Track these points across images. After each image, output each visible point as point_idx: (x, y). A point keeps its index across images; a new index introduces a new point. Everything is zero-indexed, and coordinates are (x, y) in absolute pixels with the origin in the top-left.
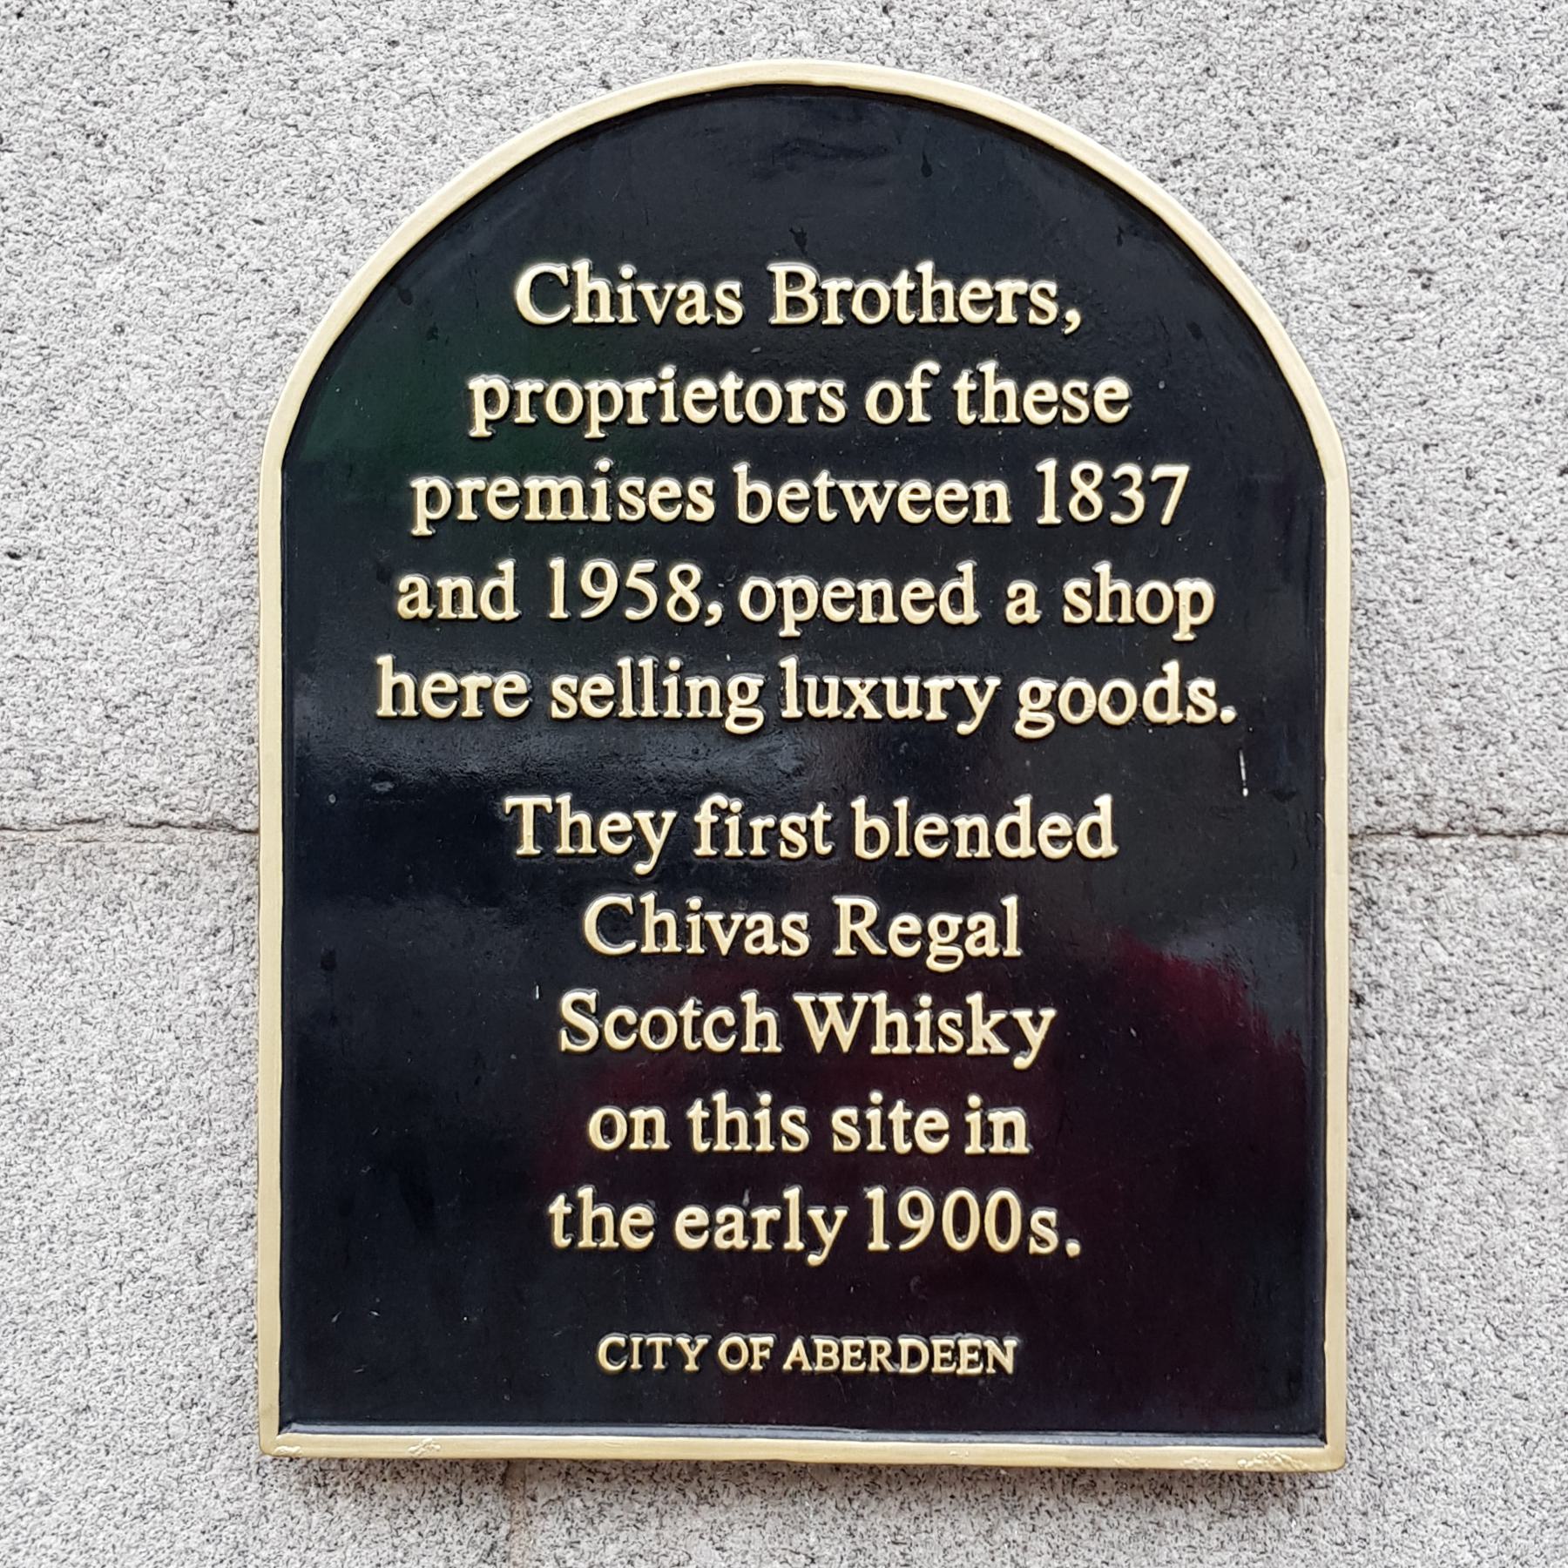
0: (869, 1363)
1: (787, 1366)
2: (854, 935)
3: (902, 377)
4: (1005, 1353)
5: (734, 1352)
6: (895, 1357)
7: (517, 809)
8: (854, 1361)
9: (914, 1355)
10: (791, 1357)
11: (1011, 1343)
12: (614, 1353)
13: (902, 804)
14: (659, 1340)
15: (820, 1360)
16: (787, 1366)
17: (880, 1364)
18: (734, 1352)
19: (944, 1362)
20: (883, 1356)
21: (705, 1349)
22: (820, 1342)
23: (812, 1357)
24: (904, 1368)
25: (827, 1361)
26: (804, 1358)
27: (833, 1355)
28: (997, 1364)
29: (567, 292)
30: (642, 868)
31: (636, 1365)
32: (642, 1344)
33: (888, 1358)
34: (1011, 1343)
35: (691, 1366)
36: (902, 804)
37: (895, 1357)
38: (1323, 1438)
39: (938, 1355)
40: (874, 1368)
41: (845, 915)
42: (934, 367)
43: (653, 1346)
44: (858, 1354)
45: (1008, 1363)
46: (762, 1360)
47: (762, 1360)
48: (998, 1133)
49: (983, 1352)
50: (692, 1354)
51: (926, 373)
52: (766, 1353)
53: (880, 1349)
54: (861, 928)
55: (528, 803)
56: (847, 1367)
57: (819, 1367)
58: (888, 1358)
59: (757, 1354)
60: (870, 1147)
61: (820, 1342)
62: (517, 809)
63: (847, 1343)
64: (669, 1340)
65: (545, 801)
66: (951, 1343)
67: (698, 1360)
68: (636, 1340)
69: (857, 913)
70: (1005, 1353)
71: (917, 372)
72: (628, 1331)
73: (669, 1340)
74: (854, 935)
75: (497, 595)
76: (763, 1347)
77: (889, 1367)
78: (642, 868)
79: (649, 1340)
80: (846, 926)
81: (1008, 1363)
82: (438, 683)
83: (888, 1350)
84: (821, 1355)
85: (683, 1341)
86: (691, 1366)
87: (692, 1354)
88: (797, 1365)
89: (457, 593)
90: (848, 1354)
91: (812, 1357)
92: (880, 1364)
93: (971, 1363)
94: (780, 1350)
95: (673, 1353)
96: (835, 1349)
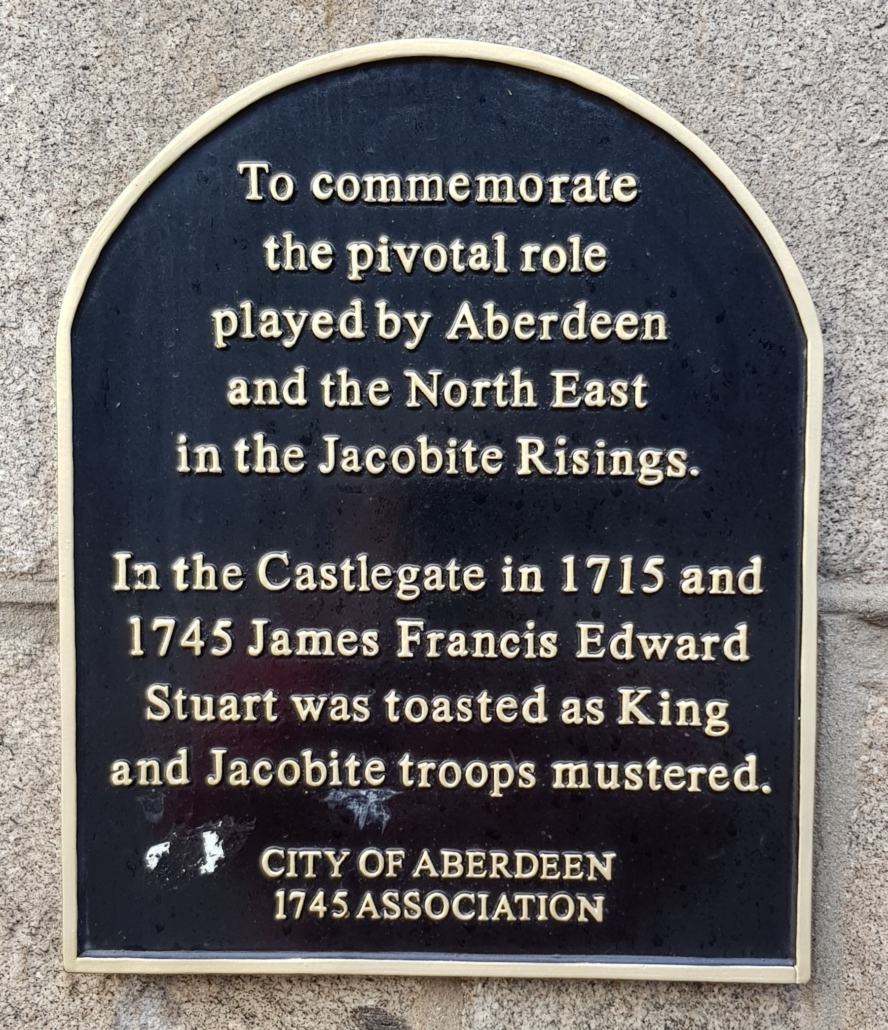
0: (563, 872)
2: (530, 461)
6: (511, 866)
8: (550, 871)
11: (609, 856)
14: (311, 854)
17: (499, 871)
18: (371, 863)
20: (501, 866)
22: (446, 854)
23: (439, 866)
25: (452, 869)
27: (458, 864)
29: (475, 906)
33: (506, 867)
34: (609, 856)
37: (511, 866)
39: (546, 866)
40: (494, 875)
41: (525, 449)
43: (305, 857)
44: (480, 864)
47: (396, 868)
48: (716, 581)
49: (586, 862)
52: (399, 863)
53: (500, 860)
54: (535, 457)
56: (470, 874)
57: (446, 874)
58: (506, 867)
59: (391, 864)
60: (468, 875)
61: (446, 854)
63: (471, 855)
64: (318, 853)
67: (340, 867)
69: (533, 447)
73: (318, 853)
74: (530, 461)
75: (293, 389)
76: (550, 861)
77: (507, 875)
80: (525, 456)
82: (346, 637)
83: (506, 861)
84: (447, 864)
85: (330, 854)
87: (337, 864)
89: (266, 388)
90: (472, 865)
91: (439, 866)
92: (499, 871)
96: (459, 858)
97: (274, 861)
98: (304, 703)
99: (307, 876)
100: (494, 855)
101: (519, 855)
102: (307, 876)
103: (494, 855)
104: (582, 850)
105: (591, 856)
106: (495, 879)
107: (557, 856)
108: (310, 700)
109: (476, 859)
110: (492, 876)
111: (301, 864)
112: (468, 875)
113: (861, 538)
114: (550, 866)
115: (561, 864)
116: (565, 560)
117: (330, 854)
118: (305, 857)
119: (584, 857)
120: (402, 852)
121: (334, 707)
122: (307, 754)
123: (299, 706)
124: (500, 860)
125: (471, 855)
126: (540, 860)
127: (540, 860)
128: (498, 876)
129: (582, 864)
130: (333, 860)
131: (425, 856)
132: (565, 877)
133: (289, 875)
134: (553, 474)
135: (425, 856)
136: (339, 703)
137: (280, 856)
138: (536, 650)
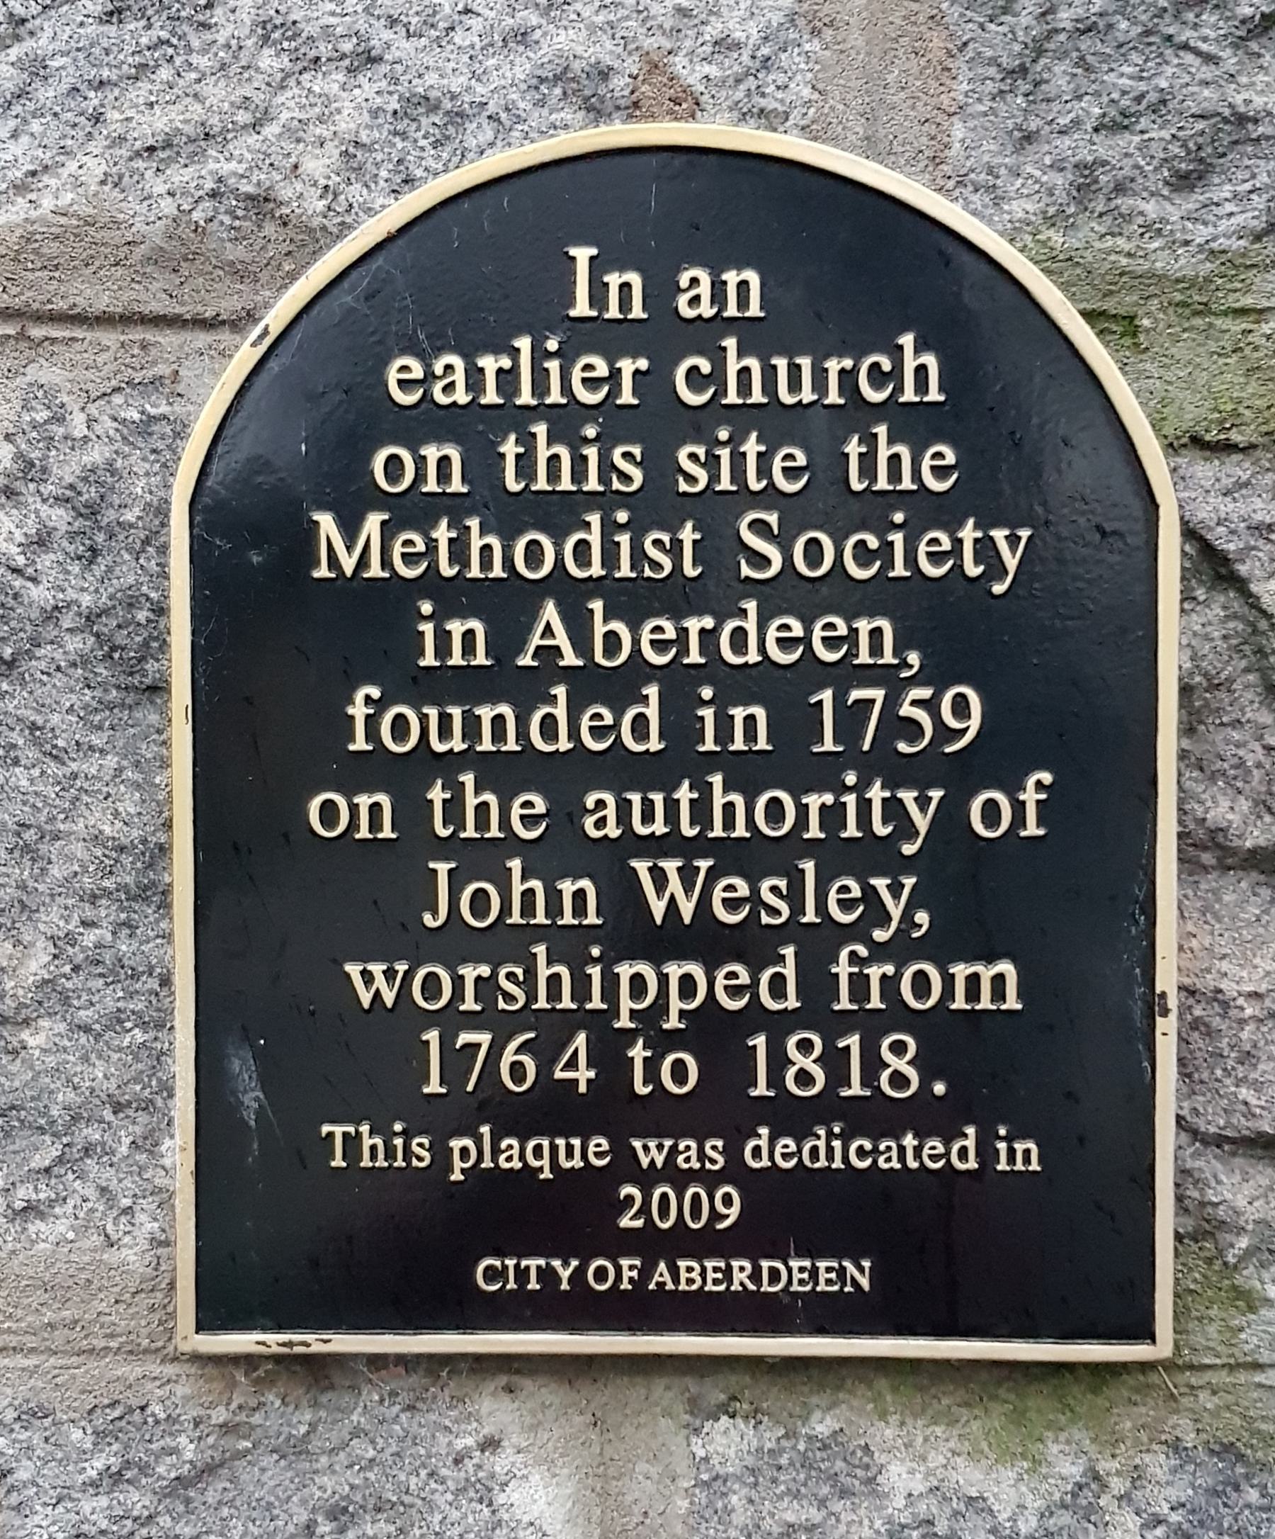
0: (817, 1284)
1: (652, 1286)
3: (1013, 788)
4: (861, 1275)
5: (601, 1274)
7: (331, 1135)
8: (716, 1282)
9: (774, 1275)
10: (656, 1278)
12: (491, 1274)
13: (485, 1130)
15: (683, 1281)
16: (652, 1286)
17: (742, 1284)
18: (601, 1274)
19: (716, 1282)
20: (743, 1276)
21: (576, 1269)
22: (682, 1264)
23: (676, 1281)
24: (766, 1288)
25: (690, 1281)
26: (667, 1278)
28: (854, 1282)
30: (909, 849)
31: (511, 1285)
32: (517, 1266)
35: (565, 1286)
36: (485, 1130)
38: (1154, 1341)
39: (797, 1276)
40: (736, 1287)
42: (1047, 778)
45: (865, 1282)
46: (631, 1280)
47: (631, 1280)
49: (842, 1272)
50: (565, 1274)
51: (1039, 784)
52: (635, 1274)
53: (742, 1269)
55: (338, 1130)
56: (709, 1287)
59: (627, 1274)
60: (706, 1289)
61: (682, 1264)
62: (331, 1135)
63: (709, 1265)
65: (351, 1129)
66: (722, 1265)
67: (570, 1280)
68: (510, 1263)
70: (861, 1275)
71: (1031, 783)
72: (500, 1253)
73: (542, 1262)
76: (631, 1268)
77: (752, 1287)
78: (909, 849)
79: (524, 1263)
81: (865, 1282)
84: (684, 1275)
85: (556, 1263)
86: (565, 1286)
87: (565, 1274)
88: (661, 1285)
90: (711, 1275)
91: (676, 1281)
92: (742, 1284)
93: (716, 1282)
94: (646, 1272)
95: (547, 1275)
97: (491, 1274)
98: (646, 1148)
99: (530, 1287)
100: (736, 1264)
101: (765, 1264)
102: (530, 1287)
103: (736, 1264)
104: (839, 1256)
105: (847, 1264)
106: (736, 1292)
107: (835, 1265)
108: (652, 1144)
109: (829, 1270)
110: (733, 1288)
111: (522, 1274)
112: (706, 1289)
113: (459, 120)
114: (688, 1275)
115: (814, 1272)
116: (510, 864)
117: (556, 1263)
118: (527, 1268)
119: (840, 1265)
120: (638, 1263)
121: (682, 1153)
122: (546, 1174)
123: (640, 1153)
124: (690, 1270)
125: (625, 1263)
126: (790, 1270)
127: (790, 1270)
128: (740, 1288)
129: (810, 1272)
130: (560, 1270)
131: (662, 1266)
132: (819, 1289)
133: (508, 1287)
134: (861, 1009)
135: (662, 1266)
136: (688, 1148)
137: (497, 1268)
138: (775, 1079)
